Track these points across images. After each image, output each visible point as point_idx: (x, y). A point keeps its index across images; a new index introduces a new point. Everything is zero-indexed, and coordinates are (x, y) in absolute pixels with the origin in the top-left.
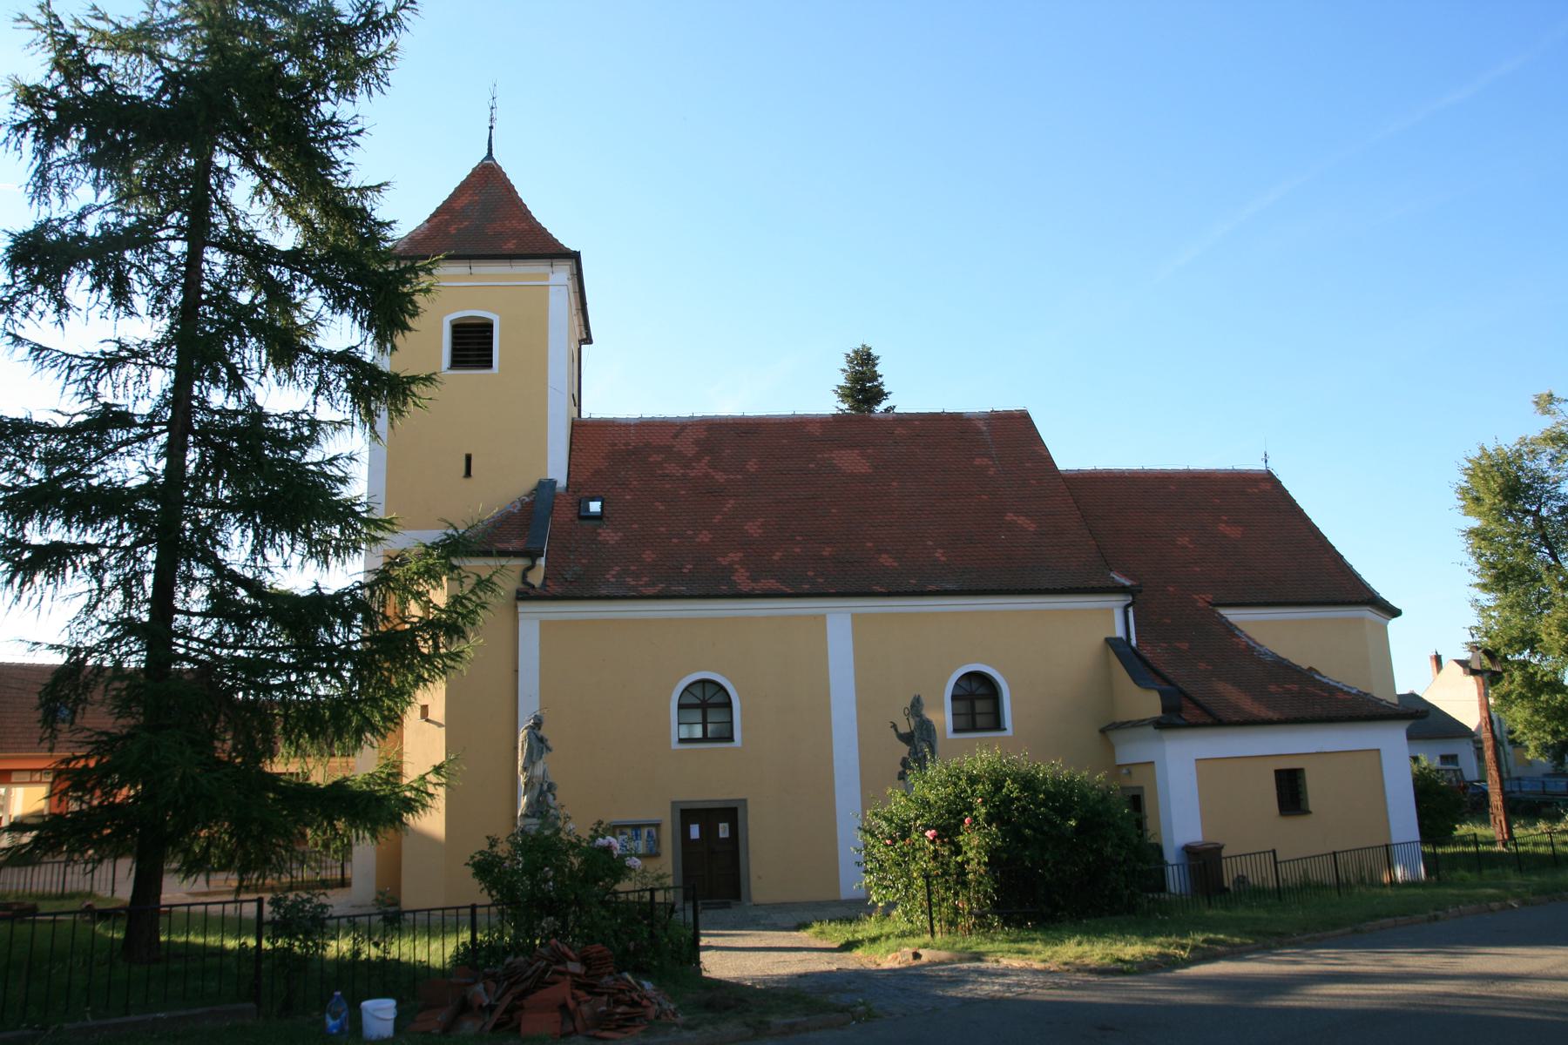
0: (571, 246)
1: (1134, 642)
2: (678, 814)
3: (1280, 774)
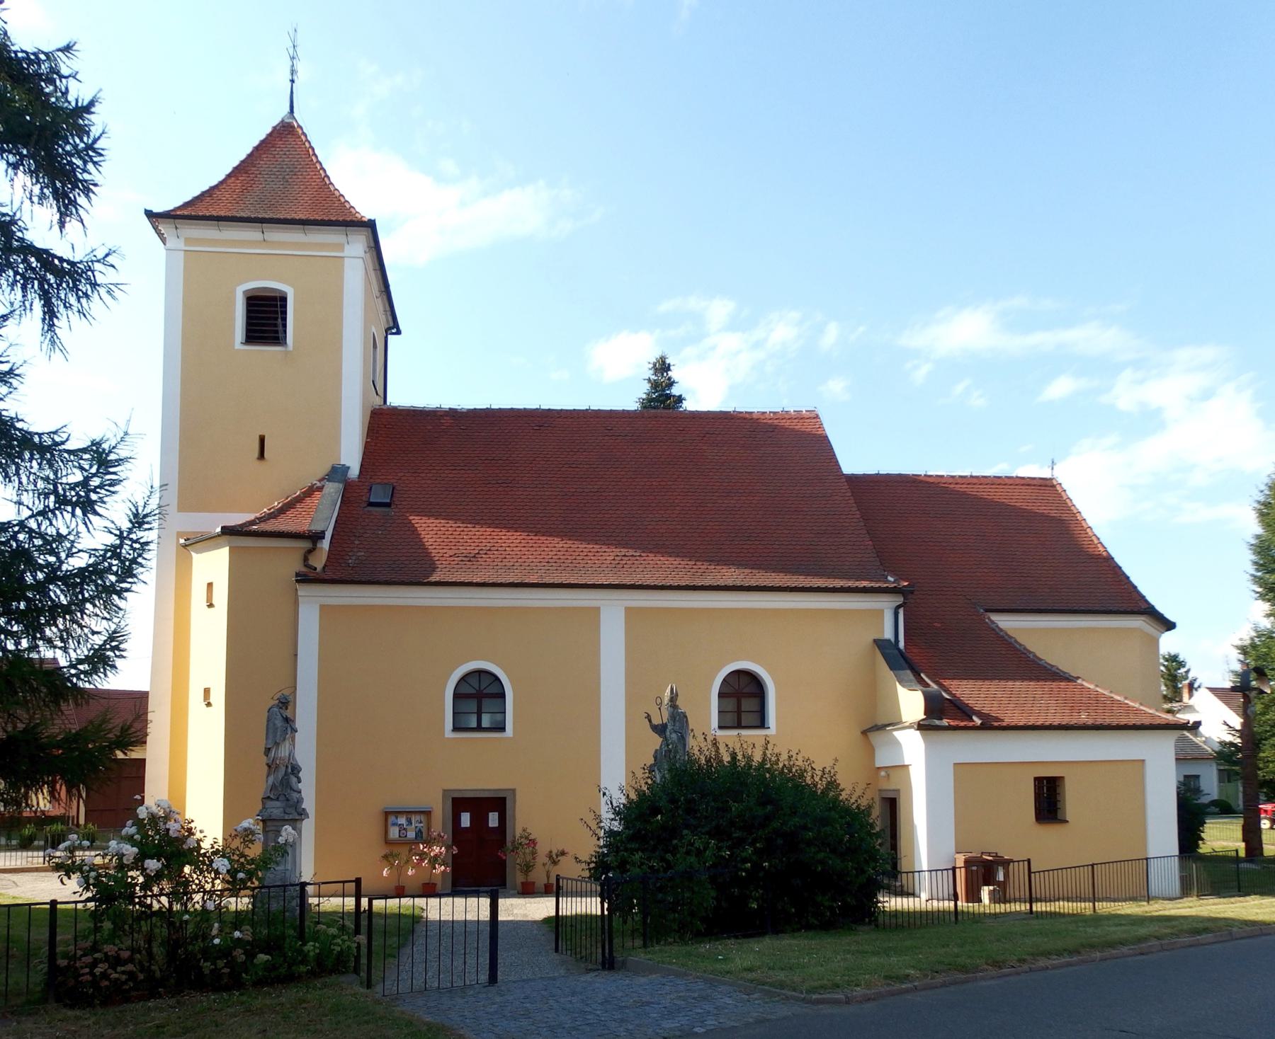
0: (366, 212)
1: (902, 645)
2: (449, 803)
3: (1038, 781)
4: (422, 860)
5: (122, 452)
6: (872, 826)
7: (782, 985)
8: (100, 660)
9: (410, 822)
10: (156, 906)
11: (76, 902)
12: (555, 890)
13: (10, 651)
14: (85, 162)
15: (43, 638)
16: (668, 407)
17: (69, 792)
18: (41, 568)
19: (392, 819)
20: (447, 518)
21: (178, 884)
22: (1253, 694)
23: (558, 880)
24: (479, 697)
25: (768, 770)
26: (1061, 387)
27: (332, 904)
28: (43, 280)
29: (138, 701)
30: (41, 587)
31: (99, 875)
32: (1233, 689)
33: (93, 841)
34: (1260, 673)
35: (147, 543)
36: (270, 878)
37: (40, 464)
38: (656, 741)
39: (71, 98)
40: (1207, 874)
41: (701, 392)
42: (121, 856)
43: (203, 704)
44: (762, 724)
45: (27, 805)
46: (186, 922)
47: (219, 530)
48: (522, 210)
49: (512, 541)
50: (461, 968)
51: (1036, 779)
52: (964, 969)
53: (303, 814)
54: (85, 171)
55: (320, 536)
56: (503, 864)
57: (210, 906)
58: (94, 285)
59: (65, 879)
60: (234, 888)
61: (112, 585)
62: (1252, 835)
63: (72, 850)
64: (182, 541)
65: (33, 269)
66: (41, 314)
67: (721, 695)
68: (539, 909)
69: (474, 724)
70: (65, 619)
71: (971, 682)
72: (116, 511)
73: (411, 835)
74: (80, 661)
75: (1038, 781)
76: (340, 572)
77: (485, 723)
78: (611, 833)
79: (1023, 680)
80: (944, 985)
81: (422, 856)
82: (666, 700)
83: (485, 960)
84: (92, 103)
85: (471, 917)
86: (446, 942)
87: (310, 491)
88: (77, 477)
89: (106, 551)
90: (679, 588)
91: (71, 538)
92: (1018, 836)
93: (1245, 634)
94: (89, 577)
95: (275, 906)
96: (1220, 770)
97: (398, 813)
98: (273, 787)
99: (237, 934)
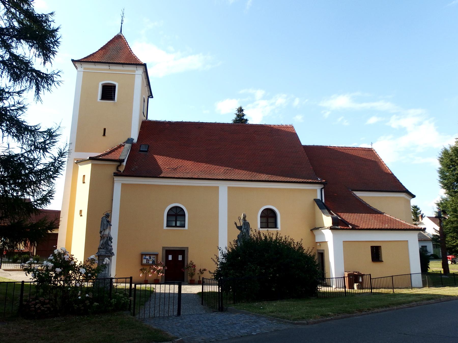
0: (143, 61)
1: (324, 201)
2: (165, 252)
3: (372, 247)
4: (154, 271)
5: (58, 133)
6: (315, 262)
7: (284, 318)
8: (45, 200)
9: (150, 258)
10: (59, 284)
11: (31, 282)
12: (202, 283)
13: (15, 196)
14: (54, 45)
15: (26, 192)
16: (242, 123)
17: (31, 244)
18: (27, 169)
19: (144, 256)
20: (167, 156)
21: (67, 277)
22: (442, 219)
23: (203, 279)
24: (176, 216)
25: (278, 243)
26: (373, 120)
27: (121, 286)
28: (37, 79)
29: (57, 214)
30: (27, 175)
31: (40, 273)
32: (436, 217)
33: (38, 261)
34: (444, 212)
35: (64, 162)
36: (100, 276)
37: (30, 136)
38: (239, 232)
39: (51, 27)
40: (431, 279)
41: (254, 118)
42: (47, 266)
43: (79, 216)
44: (276, 227)
45: (16, 248)
46: (69, 290)
47: (88, 158)
48: (195, 62)
49: (188, 164)
50: (167, 309)
51: (371, 247)
52: (349, 312)
53: (112, 254)
54: (53, 48)
55: (123, 161)
56: (183, 273)
57: (78, 285)
58: (53, 81)
59: (27, 274)
60: (87, 279)
61: (51, 175)
62: (445, 266)
63: (30, 264)
64: (76, 161)
65: (34, 76)
66: (35, 90)
67: (261, 217)
68: (196, 289)
69: (174, 225)
70: (34, 186)
71: (348, 214)
72: (54, 151)
73: (151, 262)
74: (38, 200)
75: (372, 247)
76: (129, 172)
77: (178, 224)
78: (222, 263)
79: (365, 213)
80: (342, 318)
81: (154, 270)
82: (242, 218)
83: (176, 307)
84: (58, 29)
85: (172, 291)
86: (162, 300)
87: (120, 146)
88: (42, 140)
89: (50, 164)
90: (246, 181)
91: (38, 159)
92: (365, 266)
93: (439, 200)
94: (43, 172)
95: (101, 286)
96: (433, 244)
97: (146, 255)
98: (102, 244)
99: (87, 295)
